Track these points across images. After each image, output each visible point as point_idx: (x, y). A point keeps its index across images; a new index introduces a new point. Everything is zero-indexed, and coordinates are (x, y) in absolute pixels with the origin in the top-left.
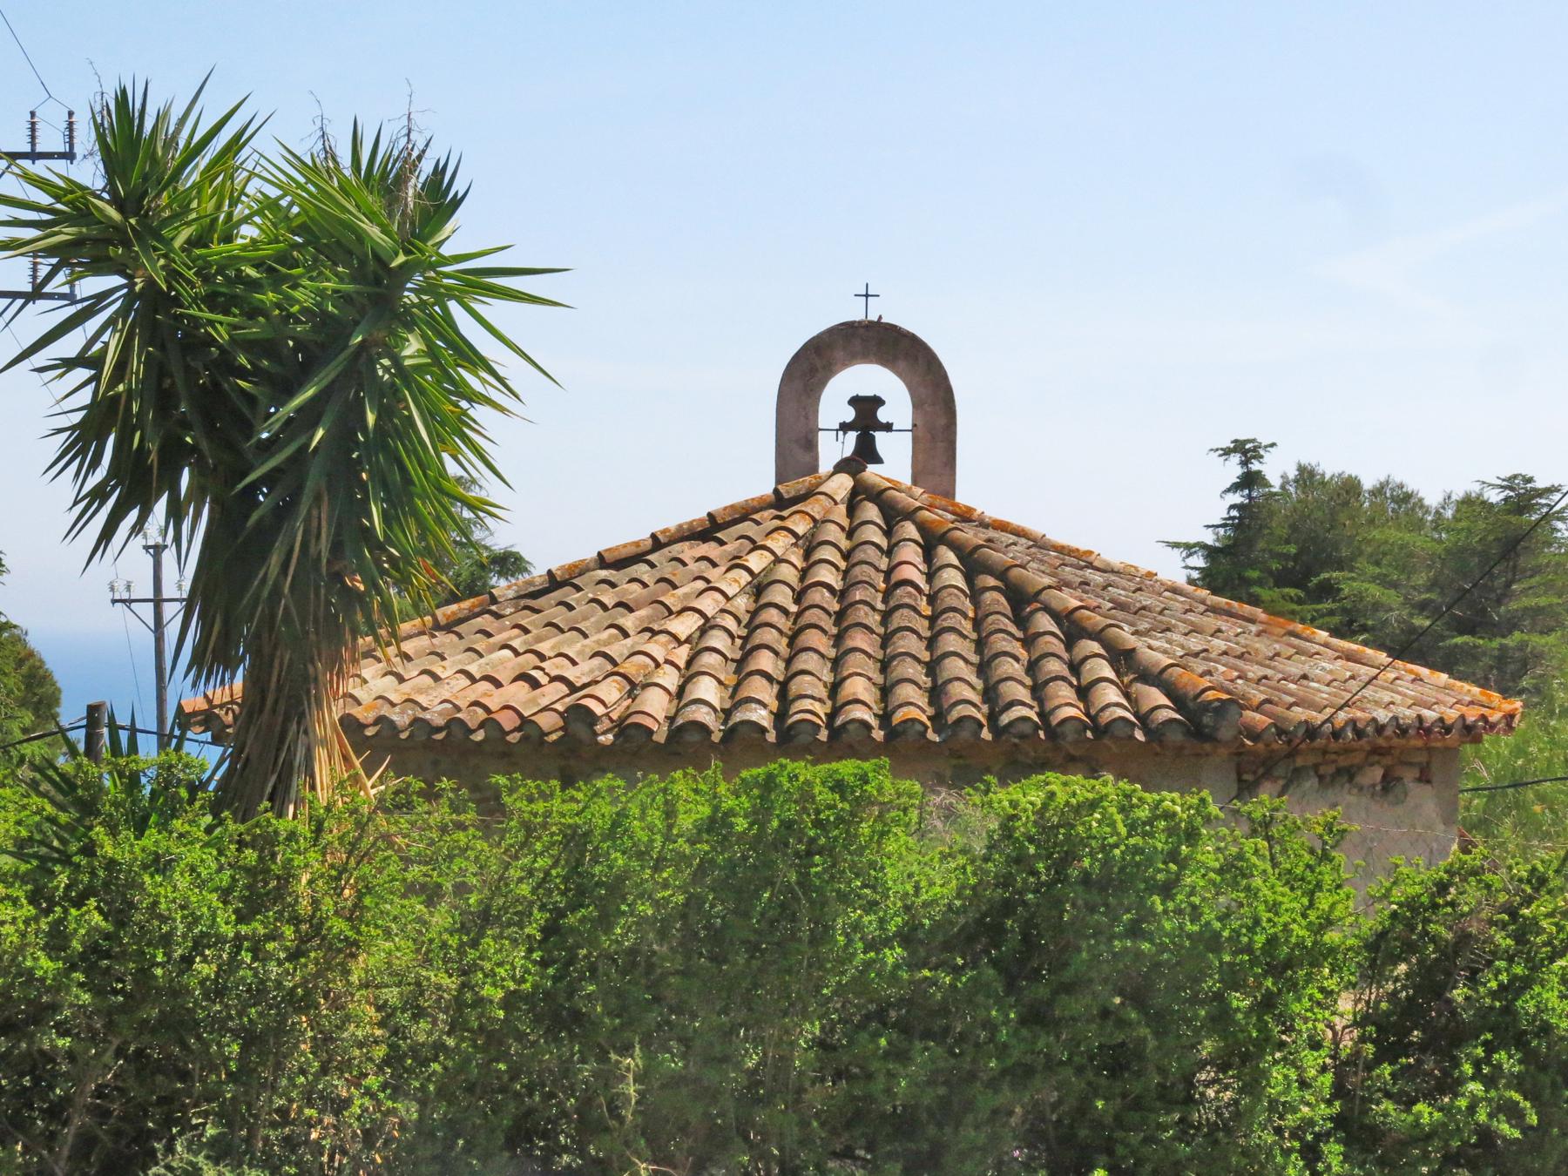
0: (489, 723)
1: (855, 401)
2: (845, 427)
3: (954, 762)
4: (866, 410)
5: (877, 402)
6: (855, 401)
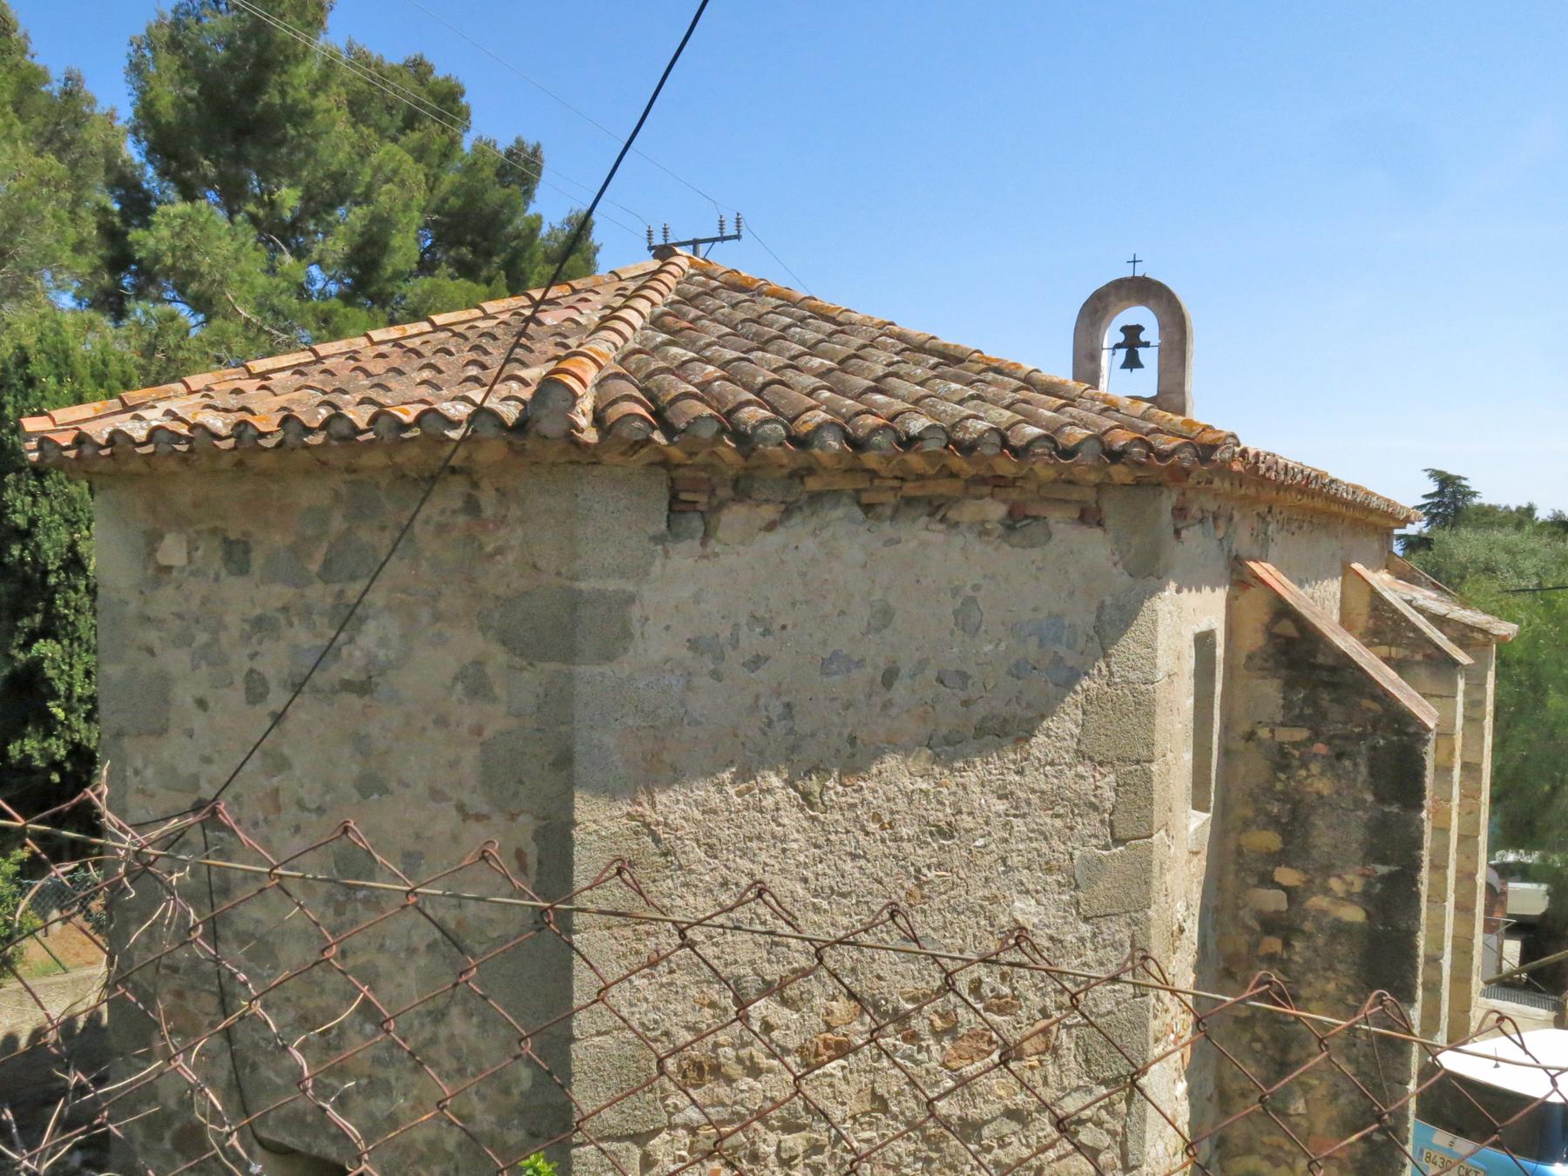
0: (81, 440)
1: (1125, 329)
2: (1118, 346)
3: (347, 477)
4: (1132, 336)
5: (1139, 329)
6: (1125, 329)
